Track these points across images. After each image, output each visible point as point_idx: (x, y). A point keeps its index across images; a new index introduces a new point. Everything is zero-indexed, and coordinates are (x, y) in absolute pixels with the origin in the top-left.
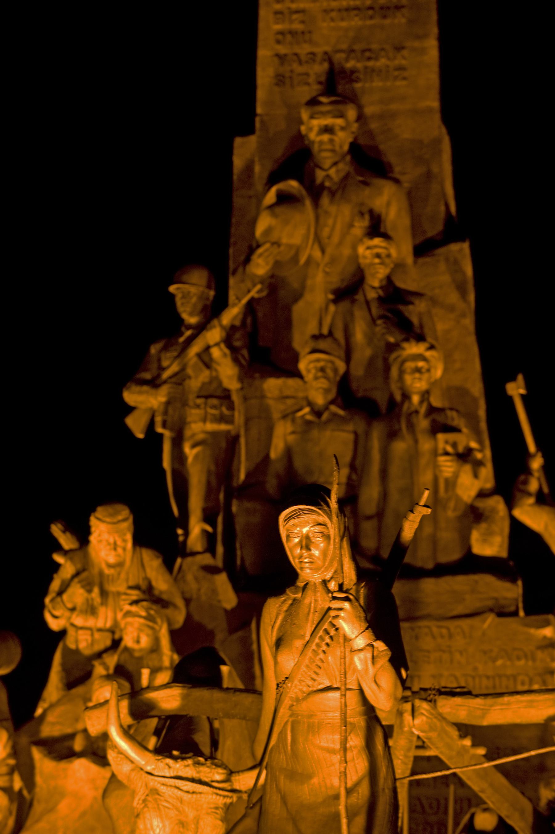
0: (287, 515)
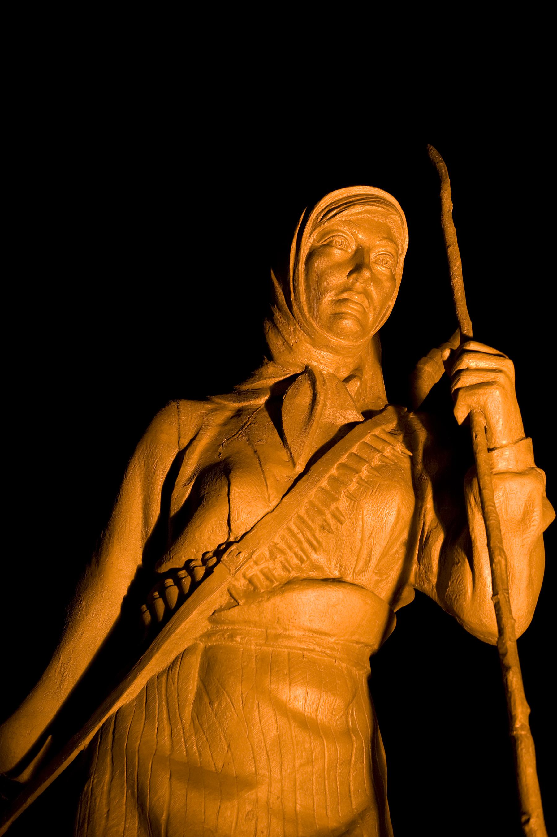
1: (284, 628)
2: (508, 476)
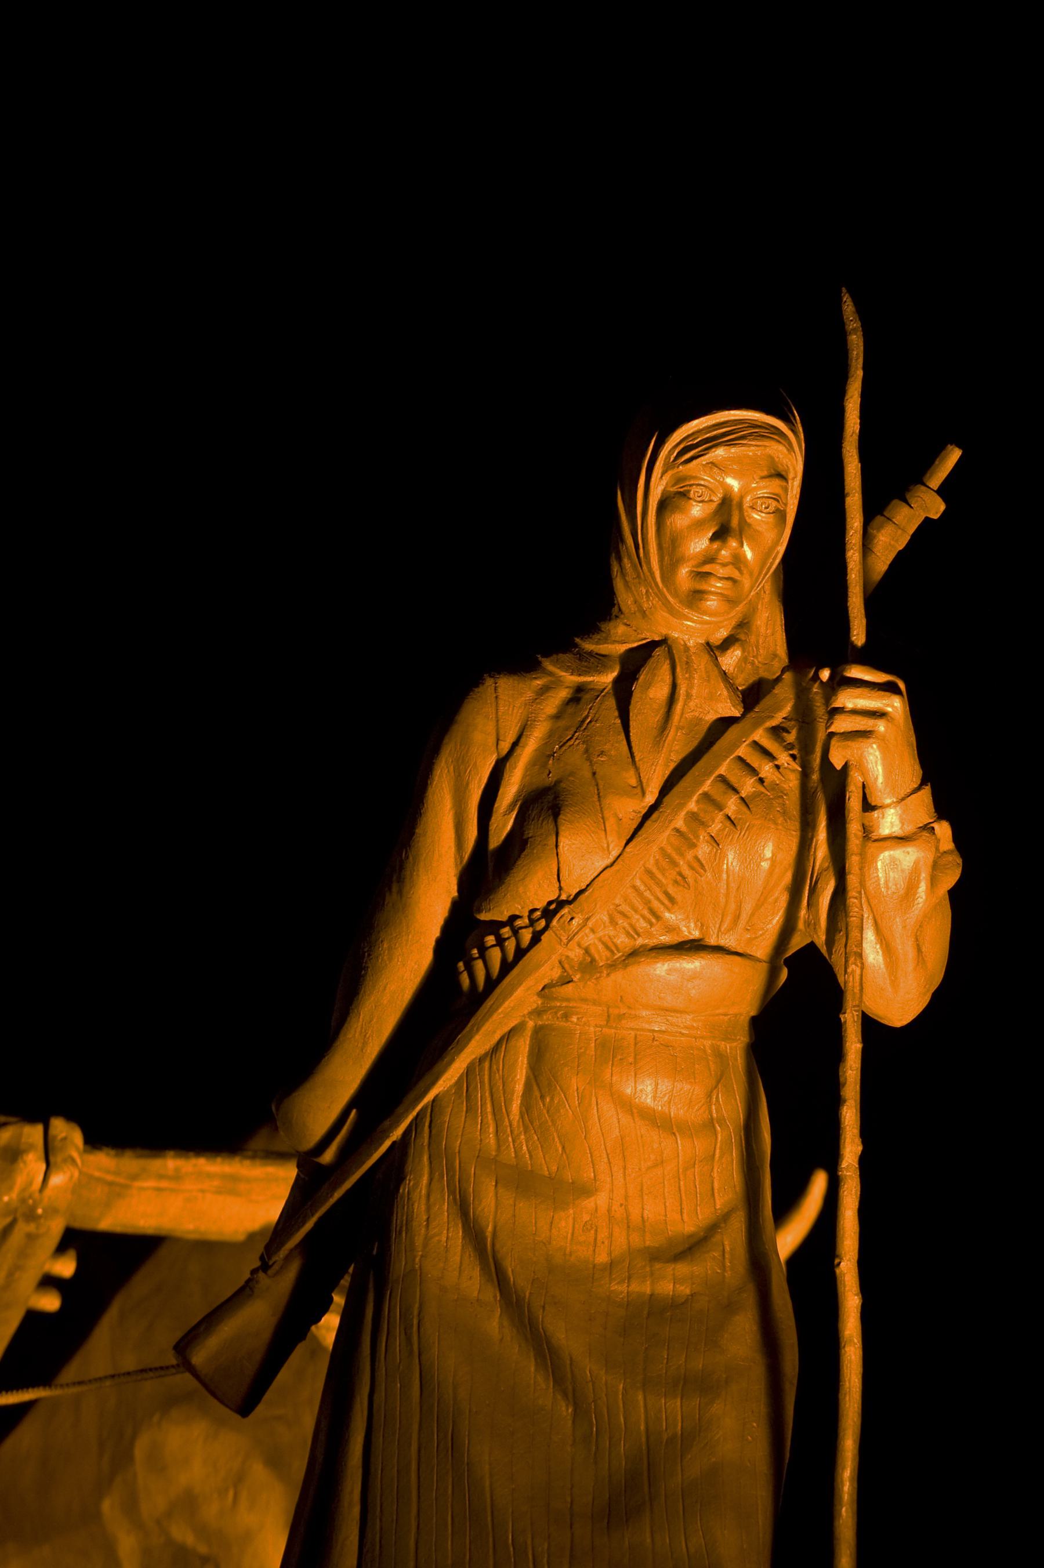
0: (699, 431)
1: (629, 1008)
2: (888, 843)
